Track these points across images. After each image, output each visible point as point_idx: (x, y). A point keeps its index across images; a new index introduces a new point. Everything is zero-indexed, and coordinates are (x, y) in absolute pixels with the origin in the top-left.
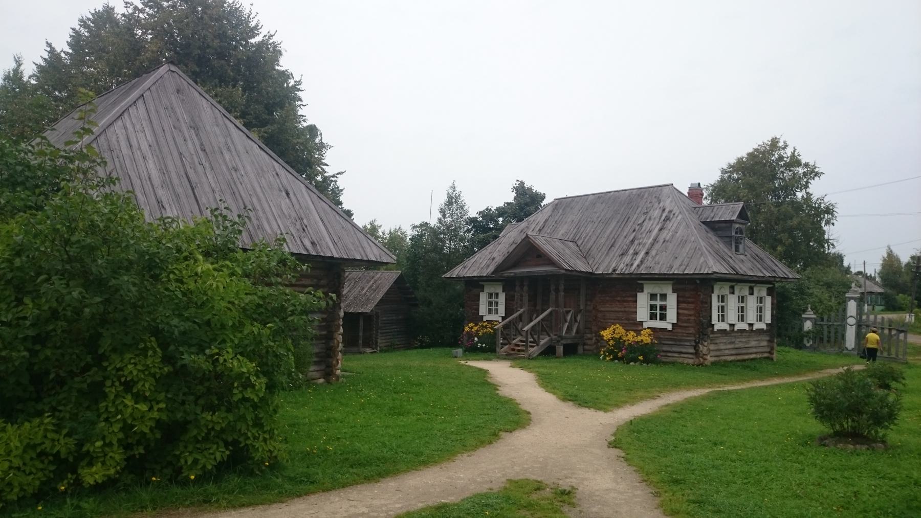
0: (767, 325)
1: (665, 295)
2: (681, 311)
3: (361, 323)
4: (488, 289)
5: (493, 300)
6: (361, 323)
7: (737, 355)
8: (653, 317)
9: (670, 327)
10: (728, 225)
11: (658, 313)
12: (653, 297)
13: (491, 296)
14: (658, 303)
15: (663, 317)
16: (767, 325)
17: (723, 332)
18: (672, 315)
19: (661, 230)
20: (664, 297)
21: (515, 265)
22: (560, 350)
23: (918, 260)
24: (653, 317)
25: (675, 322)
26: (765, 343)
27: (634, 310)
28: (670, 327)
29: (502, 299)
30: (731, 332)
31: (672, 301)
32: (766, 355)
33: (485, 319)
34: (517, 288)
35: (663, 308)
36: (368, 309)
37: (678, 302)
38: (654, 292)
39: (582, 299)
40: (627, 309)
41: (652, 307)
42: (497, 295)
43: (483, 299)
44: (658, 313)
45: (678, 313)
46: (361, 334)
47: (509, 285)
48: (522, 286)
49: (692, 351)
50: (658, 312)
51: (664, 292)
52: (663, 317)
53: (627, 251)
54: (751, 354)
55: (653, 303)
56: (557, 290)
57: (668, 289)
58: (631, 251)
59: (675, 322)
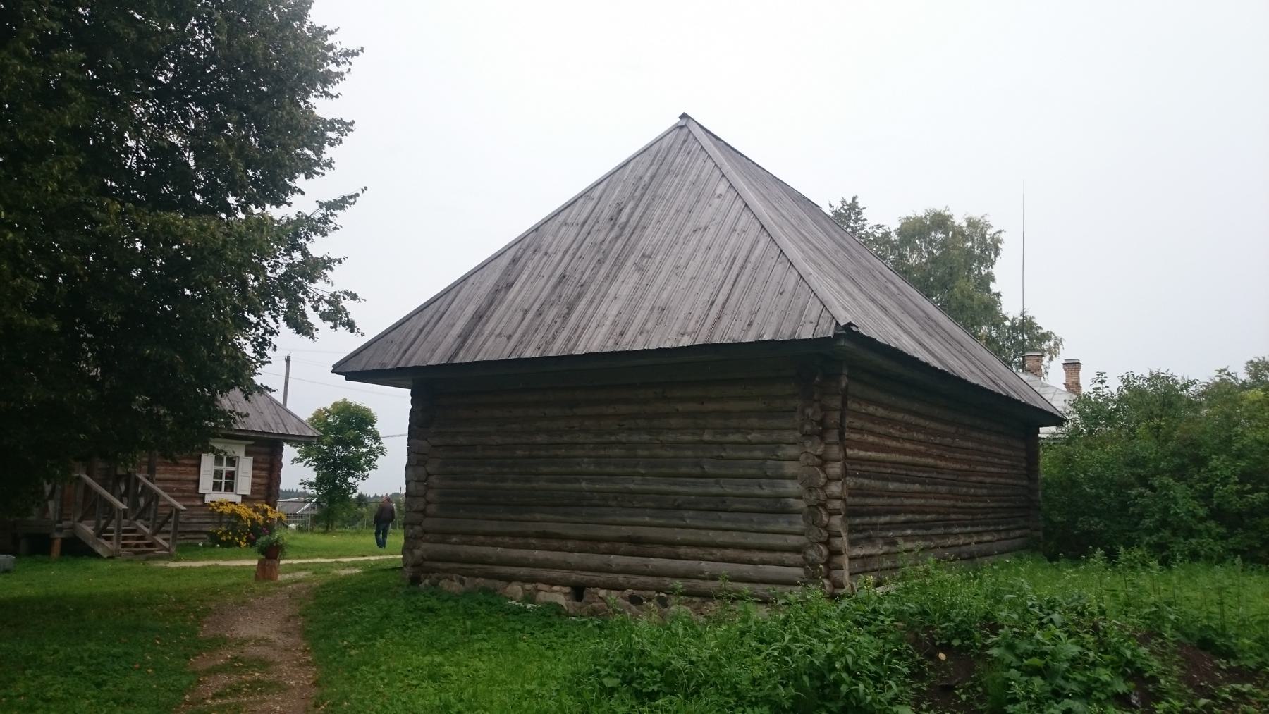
2: (195, 477)
15: (230, 487)
24: (217, 487)
25: (248, 493)
40: (184, 477)
52: (230, 487)
59: (248, 493)
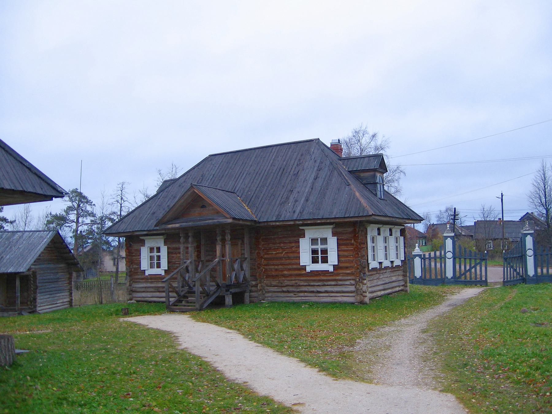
0: (402, 261)
1: (326, 239)
2: (341, 253)
3: (18, 283)
4: (150, 243)
5: (155, 254)
6: (18, 283)
7: (384, 290)
8: (315, 261)
9: (331, 269)
10: (372, 173)
11: (319, 256)
12: (314, 241)
13: (152, 250)
14: (319, 247)
15: (325, 260)
16: (402, 261)
17: (374, 269)
18: (333, 258)
19: (315, 179)
20: (324, 241)
21: (175, 219)
22: (229, 300)
23: (545, 194)
26: (401, 278)
27: (296, 255)
28: (331, 269)
29: (164, 251)
30: (380, 270)
31: (332, 245)
32: (401, 288)
33: (147, 273)
34: (182, 240)
35: (325, 252)
36: (22, 269)
37: (339, 245)
38: (315, 236)
39: (247, 248)
41: (314, 252)
42: (159, 250)
43: (145, 253)
44: (319, 256)
45: (339, 256)
46: (19, 294)
47: (170, 238)
48: (187, 237)
49: (352, 288)
50: (320, 255)
51: (325, 236)
53: (288, 198)
54: (396, 287)
55: (315, 247)
56: (223, 241)
57: (327, 232)
58: (291, 199)
